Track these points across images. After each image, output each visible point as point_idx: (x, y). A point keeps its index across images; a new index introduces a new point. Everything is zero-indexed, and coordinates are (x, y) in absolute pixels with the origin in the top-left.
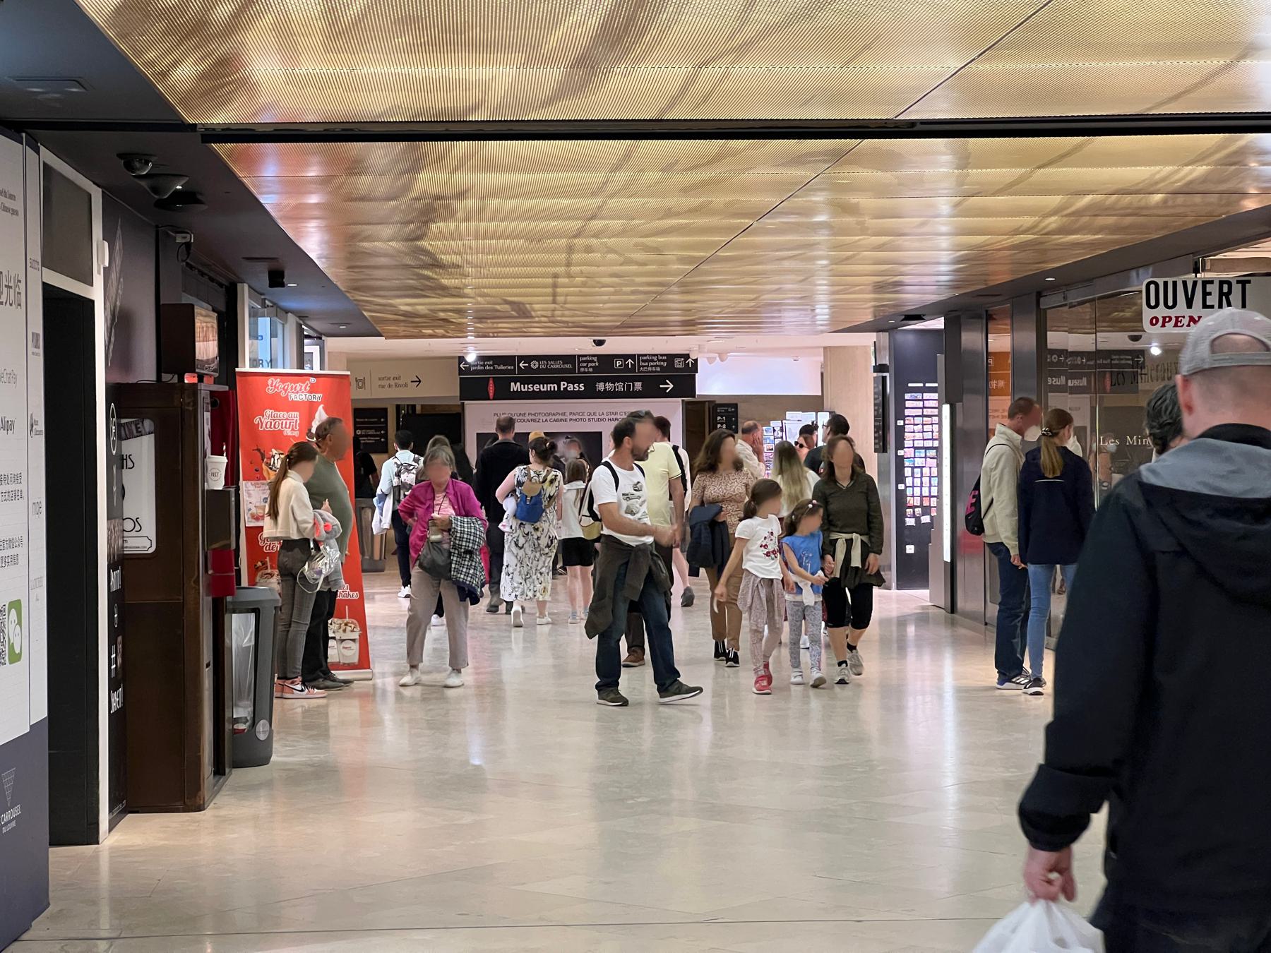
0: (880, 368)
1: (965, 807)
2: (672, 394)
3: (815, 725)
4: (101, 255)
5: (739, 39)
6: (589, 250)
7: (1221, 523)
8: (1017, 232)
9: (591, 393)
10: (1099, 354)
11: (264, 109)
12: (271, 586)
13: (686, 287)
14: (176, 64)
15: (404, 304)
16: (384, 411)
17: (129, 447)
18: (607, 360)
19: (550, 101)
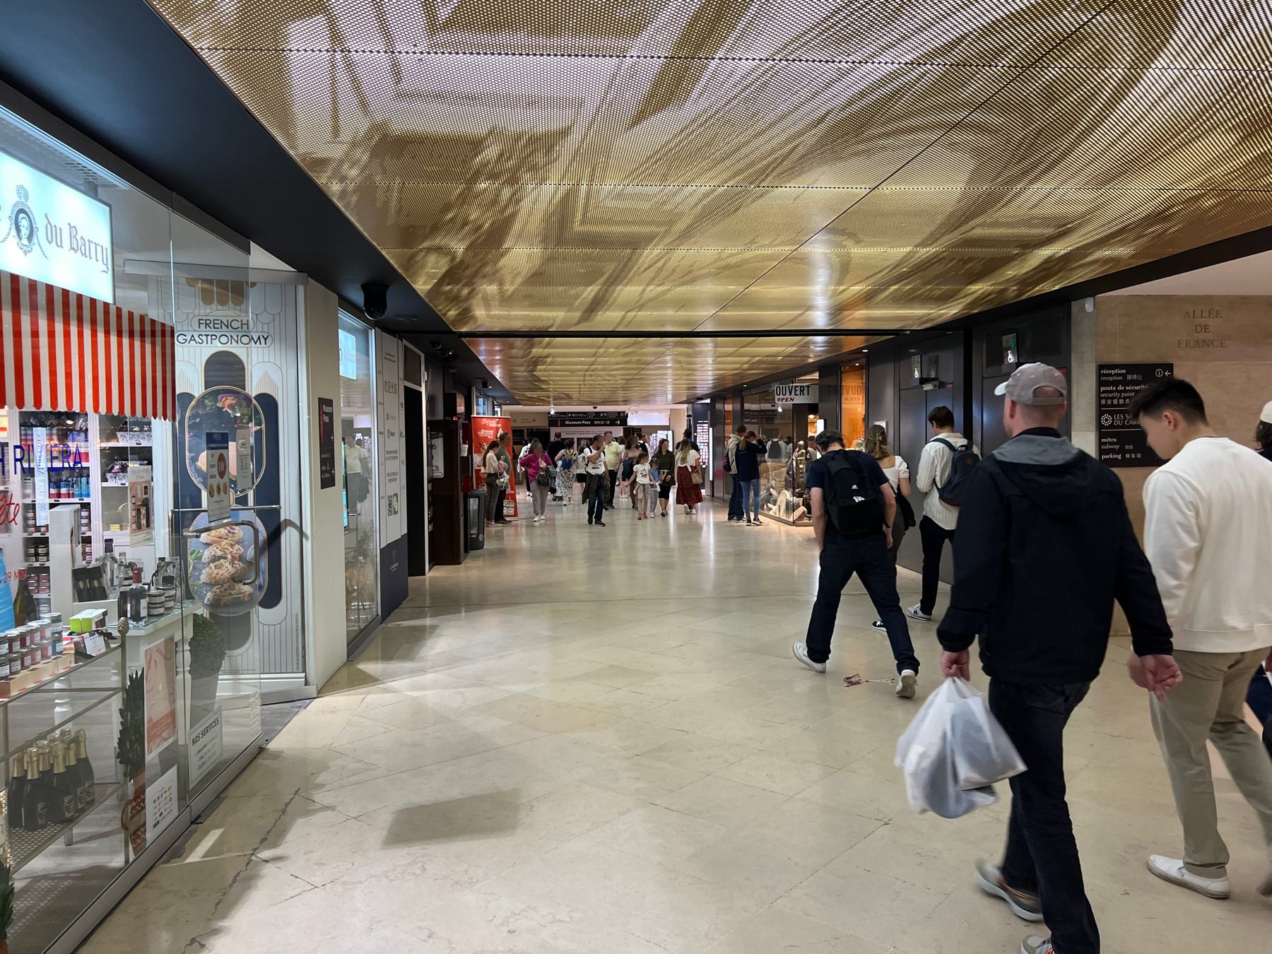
0: (688, 416)
1: (716, 561)
2: (620, 425)
3: (649, 531)
4: (424, 376)
5: (640, 303)
6: (591, 376)
7: (1043, 479)
8: (734, 369)
9: (592, 425)
10: (761, 411)
11: (479, 326)
12: (484, 489)
13: (624, 389)
14: (449, 310)
15: (529, 394)
16: (523, 431)
17: (434, 442)
18: (598, 414)
19: (579, 323)
